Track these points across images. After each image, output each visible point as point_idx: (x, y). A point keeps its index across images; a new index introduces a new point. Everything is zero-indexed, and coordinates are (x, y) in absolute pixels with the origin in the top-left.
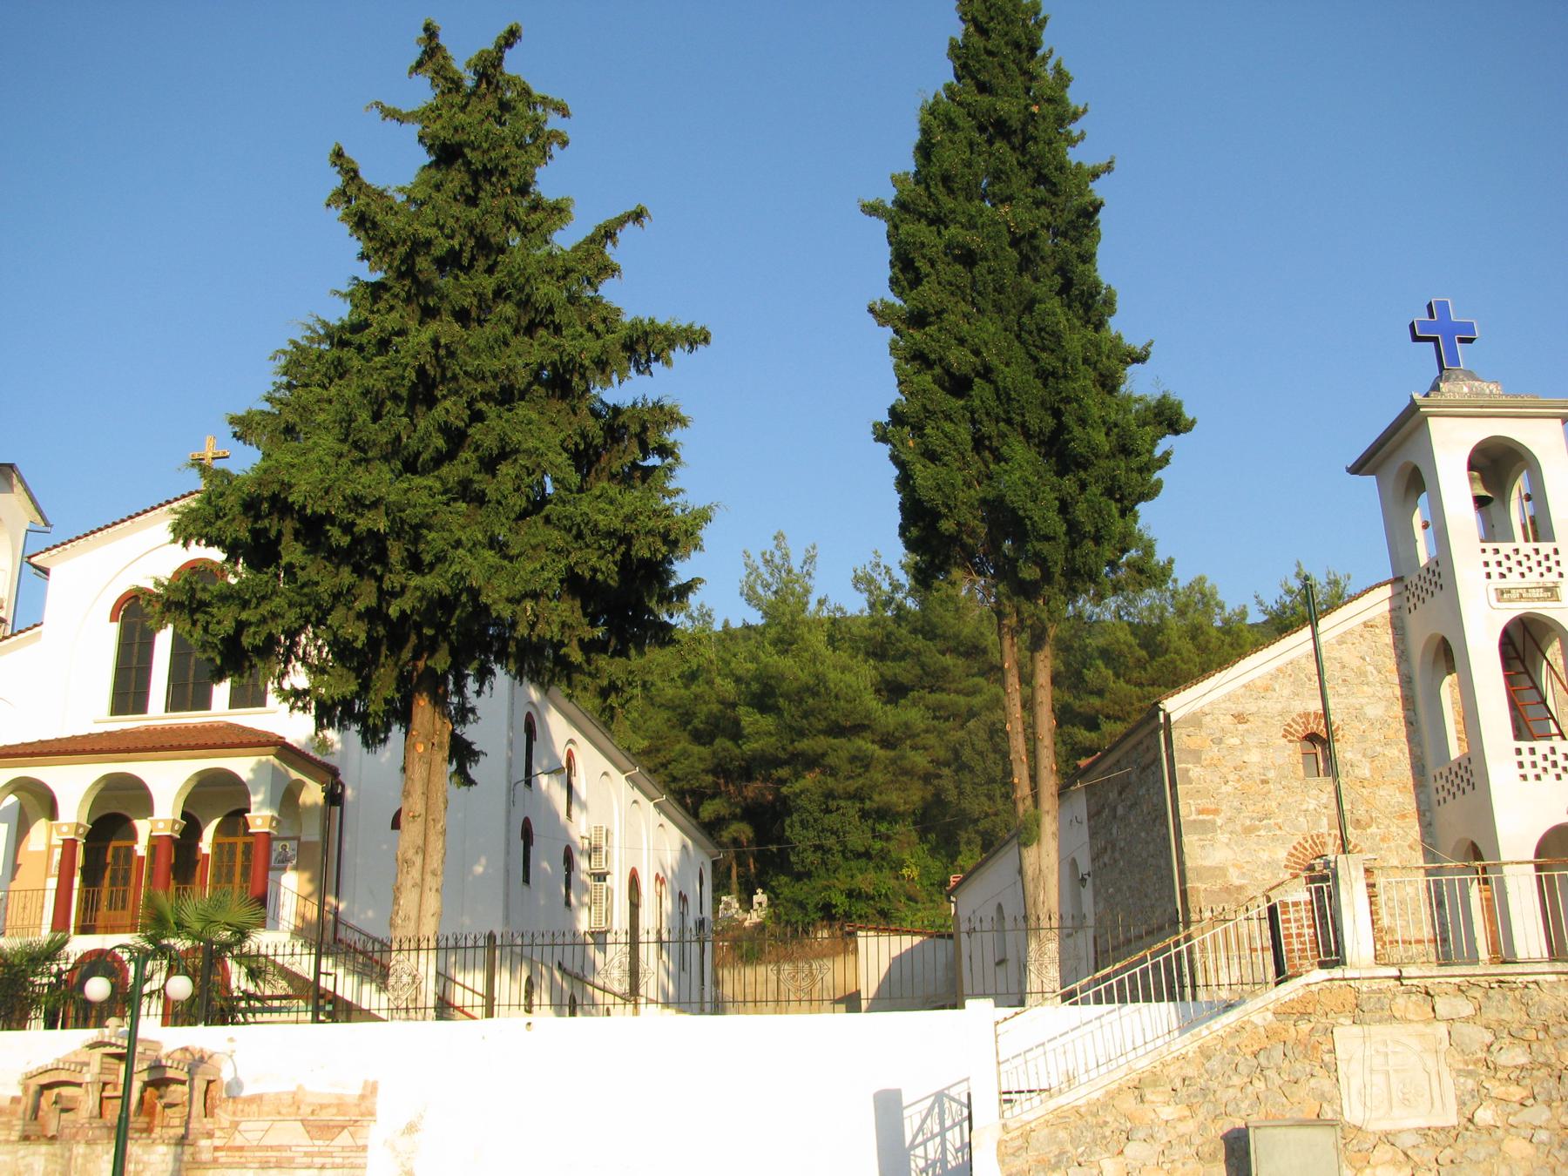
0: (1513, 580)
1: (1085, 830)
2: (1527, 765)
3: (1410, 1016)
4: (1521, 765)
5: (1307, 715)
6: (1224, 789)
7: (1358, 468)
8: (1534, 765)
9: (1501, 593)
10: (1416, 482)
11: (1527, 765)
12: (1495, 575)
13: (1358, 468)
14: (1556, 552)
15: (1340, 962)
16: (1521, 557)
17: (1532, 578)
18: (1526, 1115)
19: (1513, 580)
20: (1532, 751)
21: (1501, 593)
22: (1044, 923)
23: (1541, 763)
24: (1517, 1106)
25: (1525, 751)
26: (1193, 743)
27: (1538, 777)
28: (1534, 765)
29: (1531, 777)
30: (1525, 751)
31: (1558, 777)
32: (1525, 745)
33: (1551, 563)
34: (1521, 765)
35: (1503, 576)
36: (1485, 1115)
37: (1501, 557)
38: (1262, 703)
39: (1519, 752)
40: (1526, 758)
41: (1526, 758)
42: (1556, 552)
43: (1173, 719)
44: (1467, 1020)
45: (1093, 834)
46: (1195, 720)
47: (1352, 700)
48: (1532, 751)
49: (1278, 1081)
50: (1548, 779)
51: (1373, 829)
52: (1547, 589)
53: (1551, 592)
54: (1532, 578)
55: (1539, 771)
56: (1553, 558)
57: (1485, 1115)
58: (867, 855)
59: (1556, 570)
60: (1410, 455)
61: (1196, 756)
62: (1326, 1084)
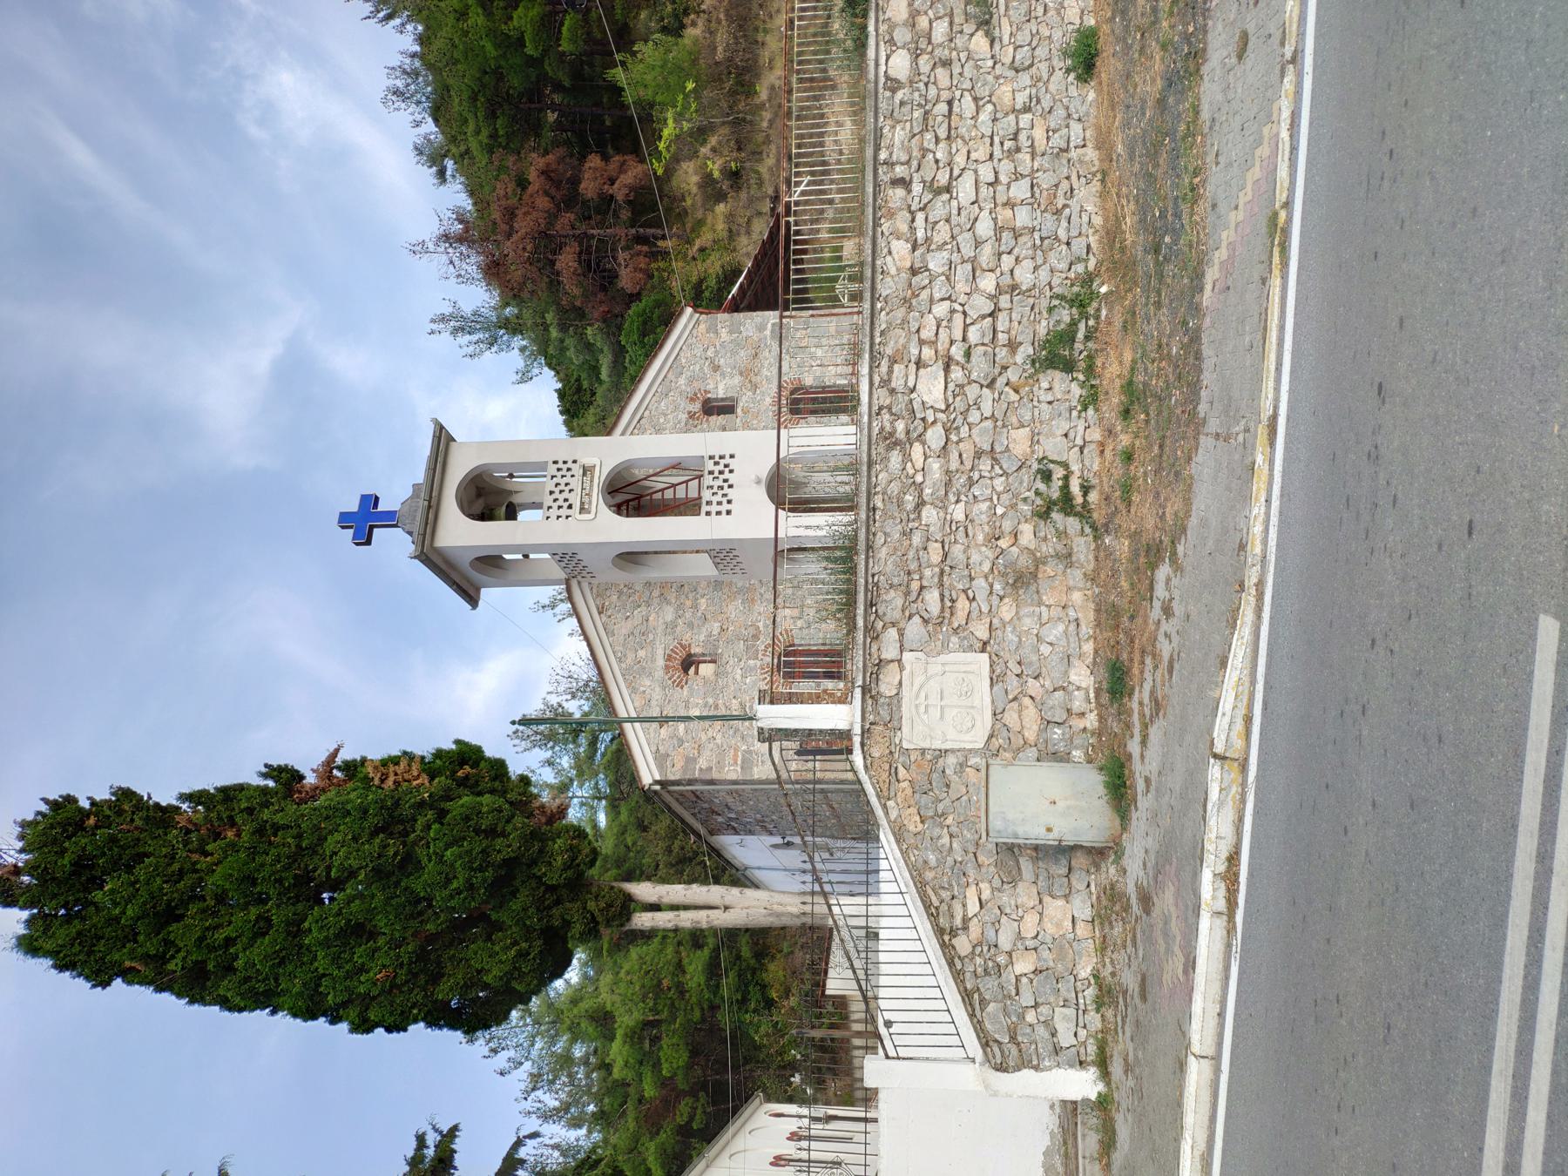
0: (575, 500)
1: (749, 839)
2: (719, 508)
3: (896, 682)
4: (719, 513)
5: (667, 667)
6: (718, 741)
7: (473, 601)
8: (719, 503)
9: (582, 510)
10: (492, 563)
11: (719, 508)
12: (569, 512)
13: (473, 601)
14: (555, 462)
15: (846, 735)
16: (557, 490)
17: (575, 483)
18: (981, 596)
19: (575, 500)
20: (708, 503)
21: (582, 510)
22: (808, 908)
23: (718, 498)
24: (974, 604)
25: (708, 508)
26: (679, 764)
27: (729, 502)
28: (719, 503)
29: (729, 507)
30: (708, 508)
31: (730, 486)
32: (705, 508)
33: (565, 467)
34: (719, 513)
35: (570, 507)
36: (981, 632)
37: (555, 505)
38: (654, 703)
39: (708, 513)
40: (714, 508)
41: (714, 508)
42: (555, 462)
43: (658, 777)
44: (901, 633)
45: (751, 833)
46: (661, 759)
47: (660, 630)
48: (708, 503)
49: (947, 802)
50: (731, 493)
51: (761, 625)
52: (584, 474)
53: (586, 470)
54: (575, 483)
55: (724, 500)
56: (560, 465)
57: (981, 632)
58: (950, 103)
59: (570, 465)
60: (465, 562)
61: (690, 761)
62: (951, 760)
